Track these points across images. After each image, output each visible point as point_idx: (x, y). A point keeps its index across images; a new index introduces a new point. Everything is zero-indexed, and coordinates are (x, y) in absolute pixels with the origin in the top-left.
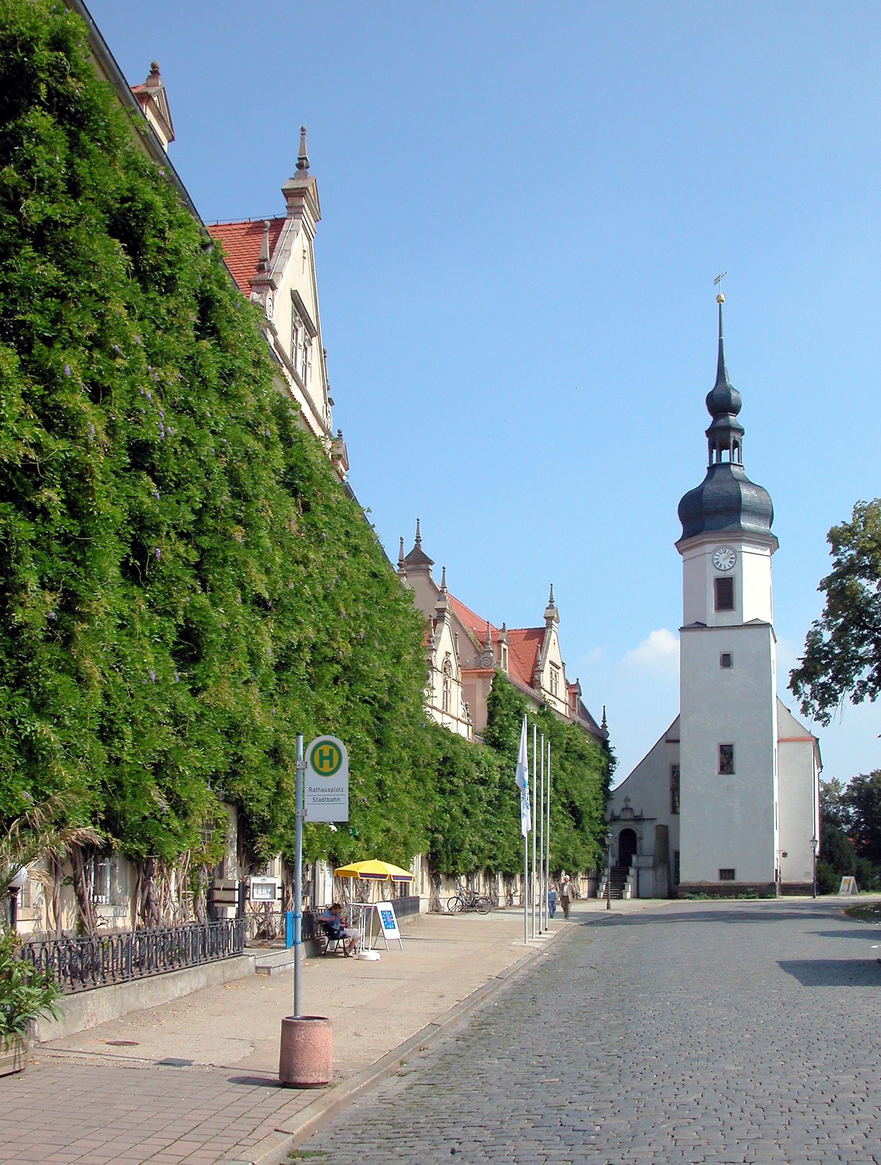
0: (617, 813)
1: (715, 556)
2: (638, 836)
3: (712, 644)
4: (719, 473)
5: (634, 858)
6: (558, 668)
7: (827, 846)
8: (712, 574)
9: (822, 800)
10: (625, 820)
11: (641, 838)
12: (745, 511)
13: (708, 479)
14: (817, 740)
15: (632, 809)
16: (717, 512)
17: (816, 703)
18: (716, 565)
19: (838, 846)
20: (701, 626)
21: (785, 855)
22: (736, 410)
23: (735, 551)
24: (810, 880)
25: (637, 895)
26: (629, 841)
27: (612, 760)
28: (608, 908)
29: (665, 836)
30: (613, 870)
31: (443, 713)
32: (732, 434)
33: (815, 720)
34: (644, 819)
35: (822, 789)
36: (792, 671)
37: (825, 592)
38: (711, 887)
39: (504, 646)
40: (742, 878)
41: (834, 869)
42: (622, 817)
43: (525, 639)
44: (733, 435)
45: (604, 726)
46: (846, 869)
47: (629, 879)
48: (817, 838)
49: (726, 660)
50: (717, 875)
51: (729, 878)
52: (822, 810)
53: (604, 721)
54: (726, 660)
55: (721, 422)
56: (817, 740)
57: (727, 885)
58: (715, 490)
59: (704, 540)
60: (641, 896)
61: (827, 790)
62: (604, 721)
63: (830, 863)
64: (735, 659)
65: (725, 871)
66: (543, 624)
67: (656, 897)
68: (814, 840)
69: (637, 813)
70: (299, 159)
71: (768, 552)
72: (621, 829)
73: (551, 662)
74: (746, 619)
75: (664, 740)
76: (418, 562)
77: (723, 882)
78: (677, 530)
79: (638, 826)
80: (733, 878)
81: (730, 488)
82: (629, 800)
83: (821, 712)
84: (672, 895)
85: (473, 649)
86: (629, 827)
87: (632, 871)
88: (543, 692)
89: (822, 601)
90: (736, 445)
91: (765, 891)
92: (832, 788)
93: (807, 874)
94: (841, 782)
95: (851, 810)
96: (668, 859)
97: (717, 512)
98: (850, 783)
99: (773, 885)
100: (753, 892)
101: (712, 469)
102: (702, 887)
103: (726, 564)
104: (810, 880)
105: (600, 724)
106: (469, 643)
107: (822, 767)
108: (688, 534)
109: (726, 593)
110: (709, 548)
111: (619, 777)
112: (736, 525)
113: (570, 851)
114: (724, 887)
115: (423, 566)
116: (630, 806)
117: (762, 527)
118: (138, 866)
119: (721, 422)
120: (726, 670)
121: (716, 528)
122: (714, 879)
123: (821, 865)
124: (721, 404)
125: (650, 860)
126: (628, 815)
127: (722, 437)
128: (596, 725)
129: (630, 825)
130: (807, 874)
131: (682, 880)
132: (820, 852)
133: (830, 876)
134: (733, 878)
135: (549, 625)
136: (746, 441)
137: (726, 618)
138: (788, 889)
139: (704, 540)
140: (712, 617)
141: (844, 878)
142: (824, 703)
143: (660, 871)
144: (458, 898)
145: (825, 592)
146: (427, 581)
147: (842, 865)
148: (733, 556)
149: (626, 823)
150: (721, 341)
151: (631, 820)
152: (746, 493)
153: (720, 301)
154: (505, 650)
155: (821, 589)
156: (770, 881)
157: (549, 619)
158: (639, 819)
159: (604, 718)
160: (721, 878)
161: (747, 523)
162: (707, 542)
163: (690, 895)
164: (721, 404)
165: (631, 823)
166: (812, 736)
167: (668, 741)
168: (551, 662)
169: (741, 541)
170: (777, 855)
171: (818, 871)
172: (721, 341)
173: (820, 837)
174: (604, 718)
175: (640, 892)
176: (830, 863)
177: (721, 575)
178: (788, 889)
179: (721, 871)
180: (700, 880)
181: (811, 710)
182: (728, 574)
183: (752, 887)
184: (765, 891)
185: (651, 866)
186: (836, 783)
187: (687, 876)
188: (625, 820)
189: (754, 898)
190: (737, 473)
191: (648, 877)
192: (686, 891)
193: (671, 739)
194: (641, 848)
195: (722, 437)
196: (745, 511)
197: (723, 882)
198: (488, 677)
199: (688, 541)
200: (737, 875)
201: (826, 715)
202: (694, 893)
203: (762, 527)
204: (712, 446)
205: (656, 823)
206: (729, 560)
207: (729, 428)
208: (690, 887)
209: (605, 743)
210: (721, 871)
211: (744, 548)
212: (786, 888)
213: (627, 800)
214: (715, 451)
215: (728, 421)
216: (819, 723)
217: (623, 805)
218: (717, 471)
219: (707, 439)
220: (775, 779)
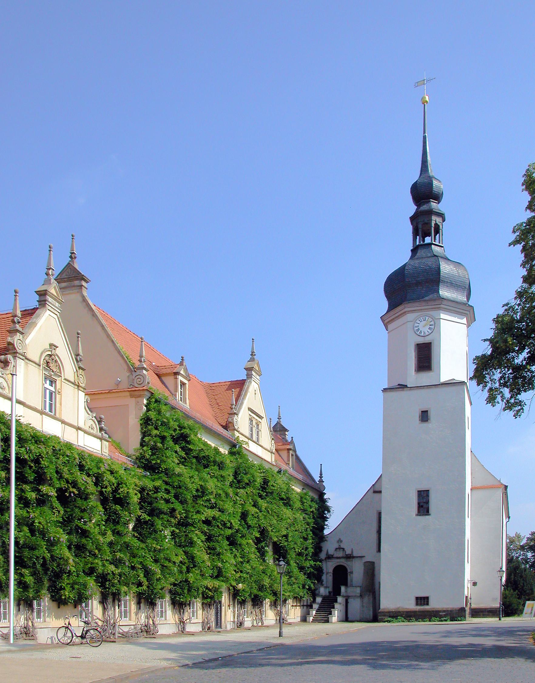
0: (331, 552)
1: (414, 323)
2: (349, 571)
3: (414, 402)
4: (421, 253)
5: (343, 589)
6: (261, 417)
7: (512, 576)
8: (413, 340)
9: (508, 549)
10: (338, 558)
11: (352, 573)
12: (444, 282)
13: (412, 258)
14: (506, 487)
15: (343, 549)
16: (418, 283)
17: (506, 392)
18: (417, 332)
19: (521, 577)
20: (403, 387)
21: (475, 584)
22: (438, 198)
23: (433, 319)
24: (496, 604)
25: (346, 619)
26: (341, 576)
27: (328, 509)
28: (280, 635)
29: (371, 571)
30: (325, 598)
31: (42, 413)
32: (434, 218)
33: (504, 410)
34: (354, 557)
35: (508, 541)
36: (477, 358)
37: (519, 247)
38: (407, 612)
39: (180, 378)
40: (434, 605)
41: (518, 595)
42: (335, 556)
43: (227, 390)
44: (435, 219)
45: (321, 481)
46: (529, 595)
47: (336, 605)
48: (504, 569)
49: (424, 416)
50: (413, 601)
51: (424, 605)
52: (508, 555)
53: (321, 477)
54: (424, 416)
55: (424, 207)
56: (506, 487)
57: (422, 611)
58: (417, 265)
59: (406, 310)
60: (349, 619)
61: (511, 541)
62: (321, 477)
63: (514, 590)
64: (432, 415)
65: (428, 496)
66: (242, 376)
67: (360, 621)
68: (501, 570)
69: (348, 552)
71: (464, 321)
72: (334, 566)
73: (250, 409)
74: (443, 379)
75: (372, 491)
76: (70, 279)
77: (419, 608)
78: (384, 304)
79: (349, 563)
80: (428, 604)
81: (430, 262)
82: (341, 541)
83: (512, 401)
84: (375, 619)
85: (126, 367)
86: (342, 564)
87: (340, 599)
88: (237, 434)
90: (437, 230)
91: (456, 615)
92: (516, 539)
93: (494, 599)
94: (522, 535)
95: (529, 555)
96: (371, 589)
97: (418, 283)
98: (529, 536)
99: (463, 610)
100: (445, 616)
101: (414, 251)
102: (399, 612)
103: (426, 330)
104: (496, 604)
105: (317, 479)
106: (122, 361)
107: (509, 518)
108: (392, 306)
109: (425, 357)
110: (410, 317)
111: (332, 523)
112: (435, 295)
113: (267, 582)
114: (419, 611)
115: (77, 283)
116: (342, 546)
117: (461, 297)
119: (424, 207)
120: (425, 425)
121: (419, 298)
122: (411, 606)
123: (507, 592)
124: (424, 193)
125: (358, 590)
126: (340, 554)
127: (424, 224)
128: (314, 480)
129: (342, 562)
130: (494, 599)
131: (382, 607)
132: (507, 581)
133: (515, 601)
134: (428, 604)
135: (249, 376)
136: (445, 228)
137: (425, 378)
138: (477, 613)
139: (406, 310)
140: (413, 377)
141: (528, 602)
142: (516, 390)
143: (366, 599)
144: (67, 628)
145: (519, 247)
146: (81, 299)
147: (525, 592)
148: (432, 323)
149: (338, 560)
150: (425, 138)
151: (343, 557)
152: (445, 268)
153: (424, 103)
154: (183, 384)
155: (516, 242)
156: (460, 606)
157: (249, 370)
158: (349, 557)
159: (321, 474)
160: (417, 604)
161: (444, 292)
162: (409, 312)
163: (389, 619)
164: (424, 193)
165: (342, 560)
166: (502, 484)
167: (375, 492)
168: (250, 409)
169: (439, 309)
170: (467, 585)
171: (504, 597)
172: (425, 138)
173: (507, 569)
174: (321, 474)
175: (349, 615)
176: (514, 590)
177: (421, 340)
178: (477, 613)
179: (417, 598)
180: (398, 606)
181: (499, 398)
182: (427, 340)
183: (444, 611)
184: (456, 615)
185: (359, 595)
186: (518, 536)
187: (387, 603)
188: (338, 558)
189: (446, 620)
190: (437, 252)
191: (355, 605)
192: (385, 615)
193: (376, 490)
194: (352, 581)
195: (424, 224)
196: (444, 282)
197: (419, 608)
198: (140, 396)
199: (392, 313)
200: (431, 601)
201: (520, 403)
202: (392, 617)
203: (461, 297)
204: (416, 233)
205: (364, 560)
206: (428, 326)
207: (431, 212)
208: (389, 612)
209: (321, 494)
210: (417, 598)
211: (442, 316)
212: (476, 612)
213: (340, 541)
214: (418, 237)
215: (430, 206)
216: (510, 414)
217: (336, 545)
218: (419, 251)
219: (411, 226)
220: (468, 521)
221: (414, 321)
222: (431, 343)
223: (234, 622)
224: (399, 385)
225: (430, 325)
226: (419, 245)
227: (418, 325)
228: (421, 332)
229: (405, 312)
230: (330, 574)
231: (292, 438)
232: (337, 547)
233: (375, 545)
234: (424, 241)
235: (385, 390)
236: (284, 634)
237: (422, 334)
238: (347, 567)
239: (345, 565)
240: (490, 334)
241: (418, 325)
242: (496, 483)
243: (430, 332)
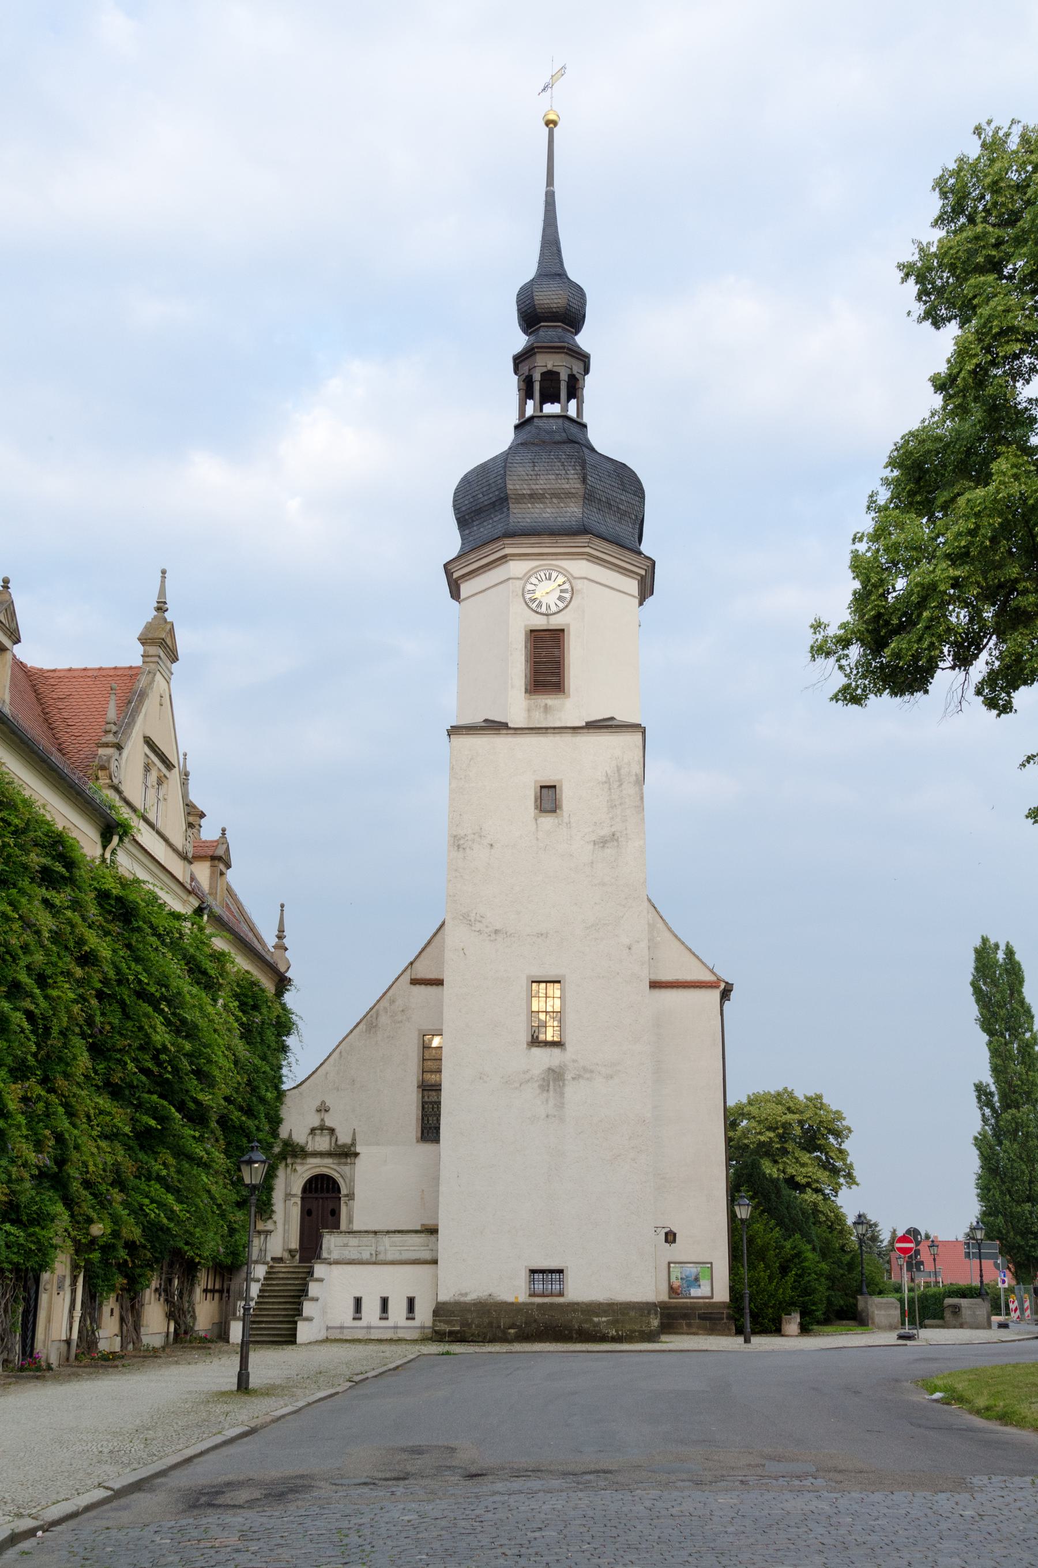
0: (300, 1137)
1: (543, 584)
2: (344, 1191)
3: (527, 761)
11: (351, 1196)
15: (332, 1131)
18: (532, 605)
20: (495, 727)
40: (582, 1288)
49: (548, 798)
54: (548, 798)
59: (507, 551)
64: (567, 796)
66: (132, 655)
69: (344, 1139)
70: (158, 602)
73: (149, 742)
75: (407, 977)
78: (451, 542)
79: (346, 1169)
86: (325, 1171)
89: (935, 204)
110: (516, 568)
116: (328, 1123)
118: (125, 1289)
126: (322, 1143)
140: (516, 705)
148: (567, 586)
151: (329, 1154)
159: (281, 930)
165: (328, 1161)
168: (149, 742)
174: (281, 930)
182: (555, 622)
199: (472, 556)
204: (527, 391)
206: (557, 594)
213: (323, 1109)
221: (526, 578)
222: (563, 630)
223: (68, 1342)
224: (486, 721)
225: (562, 591)
226: (532, 418)
227: (533, 587)
228: (540, 605)
229: (505, 556)
230: (293, 1200)
231: (224, 830)
232: (316, 1123)
233: (414, 1121)
234: (541, 410)
235: (454, 731)
236: (254, 1382)
237: (543, 610)
238: (340, 1181)
239: (336, 1175)
240: (852, 575)
241: (533, 587)
242: (709, 977)
243: (561, 605)
